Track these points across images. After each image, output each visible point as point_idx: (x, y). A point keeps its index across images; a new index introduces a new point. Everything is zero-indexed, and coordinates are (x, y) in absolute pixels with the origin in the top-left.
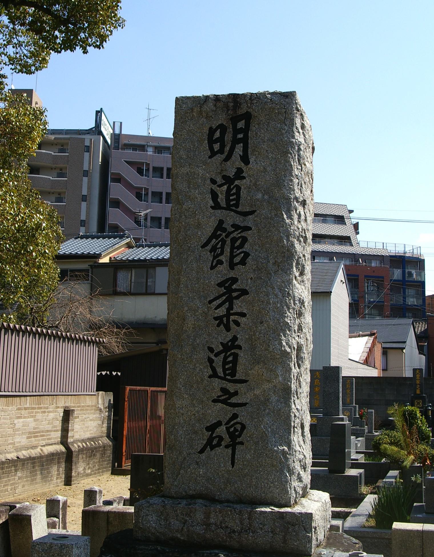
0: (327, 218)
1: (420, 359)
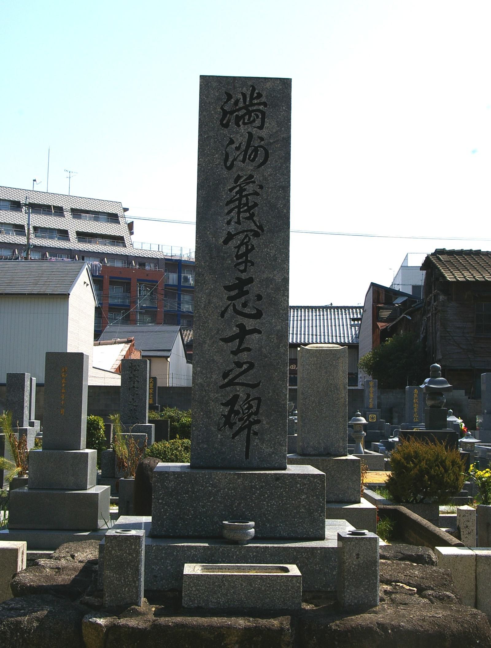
0: (99, 216)
1: (188, 367)
